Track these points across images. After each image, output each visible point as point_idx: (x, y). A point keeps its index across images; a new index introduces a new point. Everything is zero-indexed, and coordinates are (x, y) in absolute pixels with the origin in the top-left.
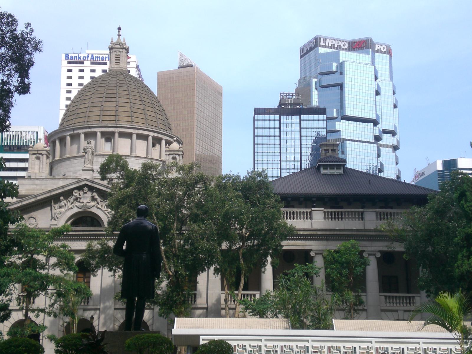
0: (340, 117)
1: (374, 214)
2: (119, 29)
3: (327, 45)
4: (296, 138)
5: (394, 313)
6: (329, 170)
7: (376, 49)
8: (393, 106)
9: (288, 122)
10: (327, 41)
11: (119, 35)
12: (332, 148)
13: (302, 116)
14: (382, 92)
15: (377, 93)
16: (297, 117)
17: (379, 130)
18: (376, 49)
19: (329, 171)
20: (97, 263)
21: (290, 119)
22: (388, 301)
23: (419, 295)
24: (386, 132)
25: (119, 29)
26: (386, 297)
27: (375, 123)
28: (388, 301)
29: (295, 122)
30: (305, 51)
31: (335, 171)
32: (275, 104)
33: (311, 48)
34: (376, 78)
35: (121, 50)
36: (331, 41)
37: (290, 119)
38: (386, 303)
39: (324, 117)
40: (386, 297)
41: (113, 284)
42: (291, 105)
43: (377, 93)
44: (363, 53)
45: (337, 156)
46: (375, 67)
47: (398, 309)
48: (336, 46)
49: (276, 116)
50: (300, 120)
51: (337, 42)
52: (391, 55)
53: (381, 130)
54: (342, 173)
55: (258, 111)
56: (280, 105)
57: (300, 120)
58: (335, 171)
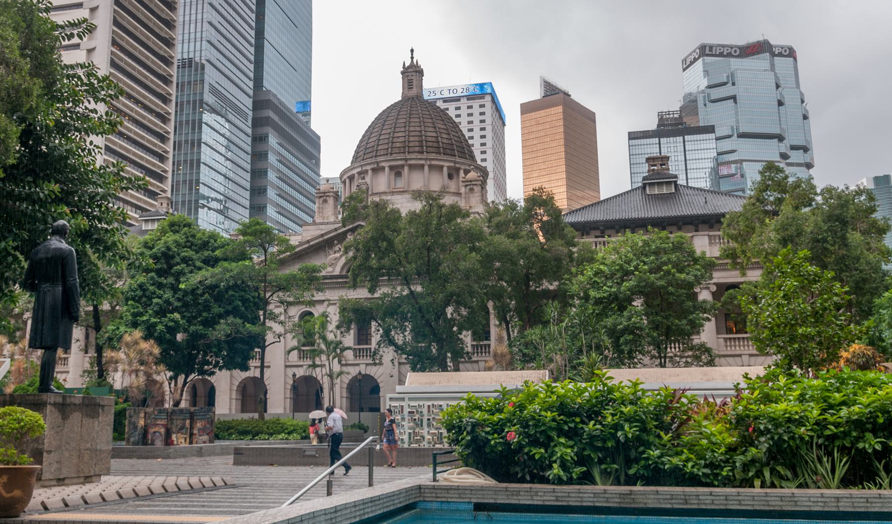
0: (736, 135)
1: (706, 238)
2: (412, 51)
3: (714, 53)
4: (680, 163)
5: (736, 358)
6: (665, 188)
7: (776, 53)
8: (802, 117)
9: (669, 145)
10: (714, 48)
11: (412, 58)
12: (660, 163)
13: (686, 137)
14: (786, 101)
15: (780, 103)
16: (680, 139)
17: (786, 146)
18: (776, 53)
19: (656, 191)
20: (227, 292)
21: (672, 141)
22: (728, 344)
23: (698, 337)
24: (793, 148)
25: (412, 51)
26: (726, 339)
27: (780, 138)
28: (728, 344)
29: (678, 145)
30: (688, 63)
31: (665, 190)
32: (652, 125)
33: (695, 58)
34: (778, 86)
35: (414, 74)
36: (718, 48)
37: (672, 141)
38: (726, 346)
39: (712, 136)
40: (726, 339)
41: (74, 314)
42: (671, 125)
43: (780, 103)
44: (758, 59)
45: (667, 172)
46: (775, 73)
47: (742, 353)
48: (725, 53)
49: (654, 139)
50: (684, 142)
51: (726, 49)
52: (795, 59)
53: (789, 146)
54: (673, 191)
55: (633, 136)
56: (659, 126)
57: (684, 142)
58: (665, 190)
